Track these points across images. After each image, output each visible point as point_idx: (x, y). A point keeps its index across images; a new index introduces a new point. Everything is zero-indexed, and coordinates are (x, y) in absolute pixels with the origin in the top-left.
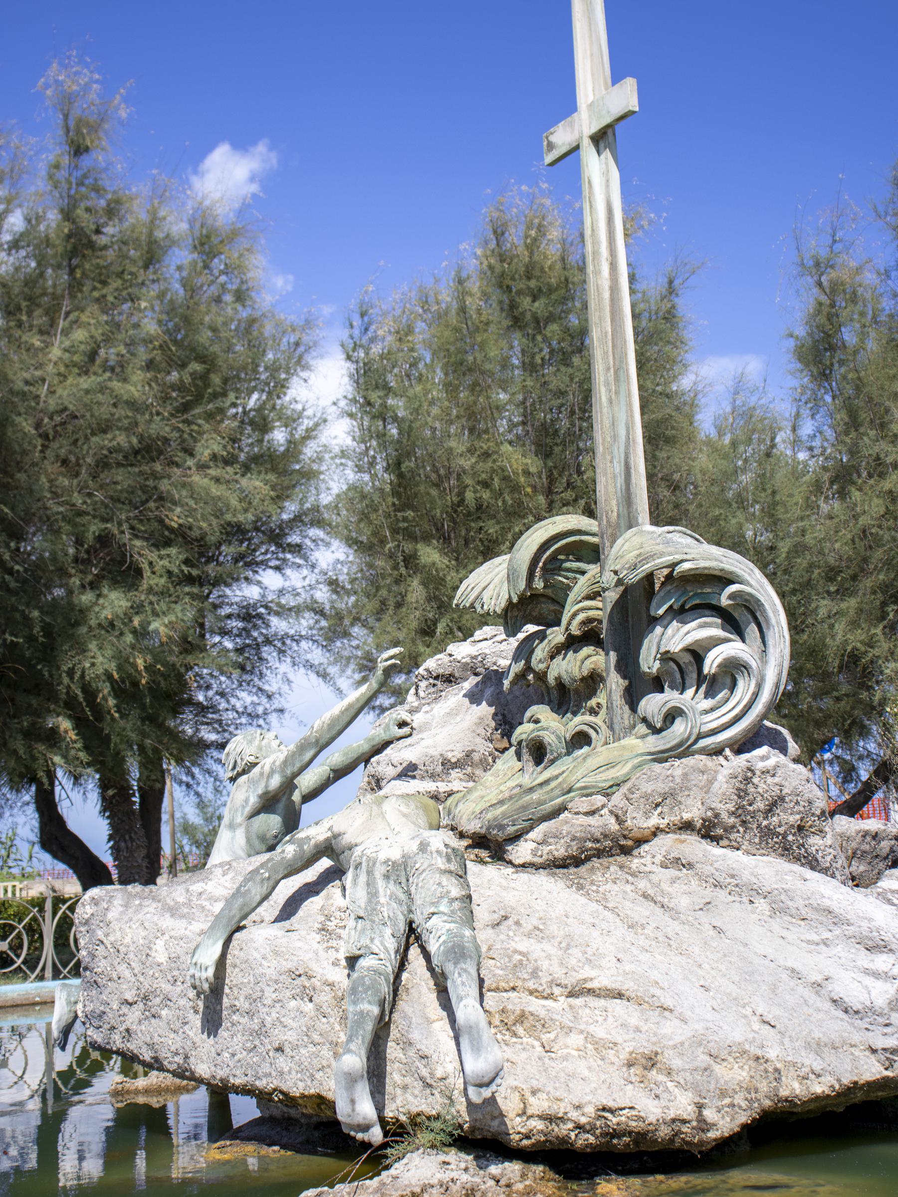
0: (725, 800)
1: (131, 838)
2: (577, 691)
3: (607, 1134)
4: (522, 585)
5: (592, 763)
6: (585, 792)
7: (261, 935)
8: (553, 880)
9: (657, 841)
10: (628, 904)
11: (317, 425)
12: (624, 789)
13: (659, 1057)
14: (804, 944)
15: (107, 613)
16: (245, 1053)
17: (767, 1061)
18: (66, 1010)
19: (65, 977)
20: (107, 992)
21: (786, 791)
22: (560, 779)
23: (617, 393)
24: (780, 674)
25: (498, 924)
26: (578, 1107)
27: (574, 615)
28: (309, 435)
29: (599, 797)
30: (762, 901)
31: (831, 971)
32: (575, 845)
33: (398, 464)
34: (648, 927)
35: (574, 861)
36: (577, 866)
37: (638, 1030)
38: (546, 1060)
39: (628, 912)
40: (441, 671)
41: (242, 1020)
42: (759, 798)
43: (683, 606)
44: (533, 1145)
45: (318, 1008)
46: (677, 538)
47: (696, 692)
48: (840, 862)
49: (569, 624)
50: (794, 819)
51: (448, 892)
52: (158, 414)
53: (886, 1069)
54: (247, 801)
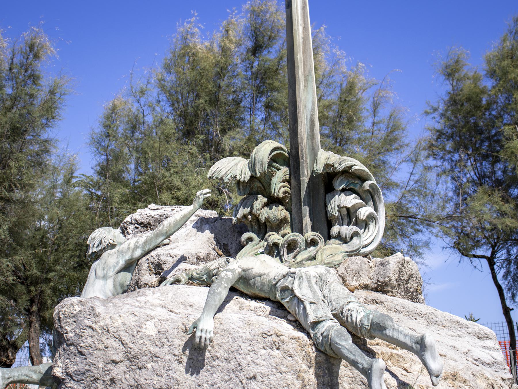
16: (222, 383)
30: (421, 319)
40: (143, 221)
41: (221, 364)
54: (117, 263)
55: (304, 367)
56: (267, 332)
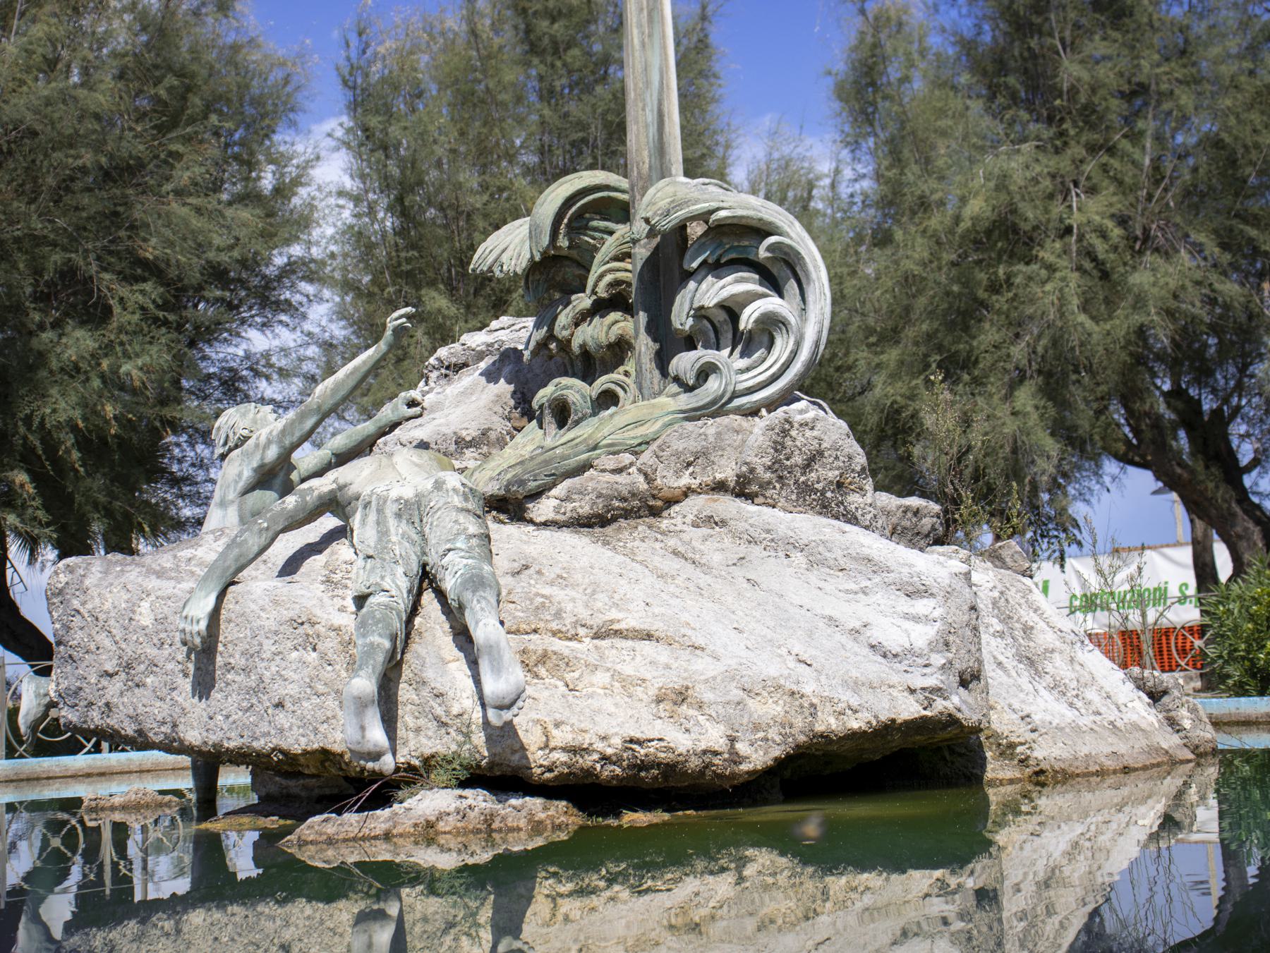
0: (761, 453)
2: (602, 359)
3: (635, 766)
4: (545, 240)
5: (620, 420)
6: (612, 449)
7: (259, 584)
12: (654, 446)
13: (690, 692)
14: (842, 594)
15: (71, 354)
16: (240, 713)
17: (802, 696)
18: (35, 703)
19: (21, 756)
20: (84, 665)
21: (824, 445)
24: (820, 332)
26: (604, 738)
28: (297, 182)
30: (799, 554)
31: (870, 616)
36: (602, 527)
37: (668, 667)
38: (570, 698)
40: (454, 360)
41: (238, 679)
42: (797, 452)
43: (718, 260)
44: (556, 777)
45: (323, 656)
46: (712, 188)
48: (880, 522)
49: (596, 285)
50: (833, 475)
51: (465, 529)
52: (131, 129)
53: (925, 709)
54: (240, 475)
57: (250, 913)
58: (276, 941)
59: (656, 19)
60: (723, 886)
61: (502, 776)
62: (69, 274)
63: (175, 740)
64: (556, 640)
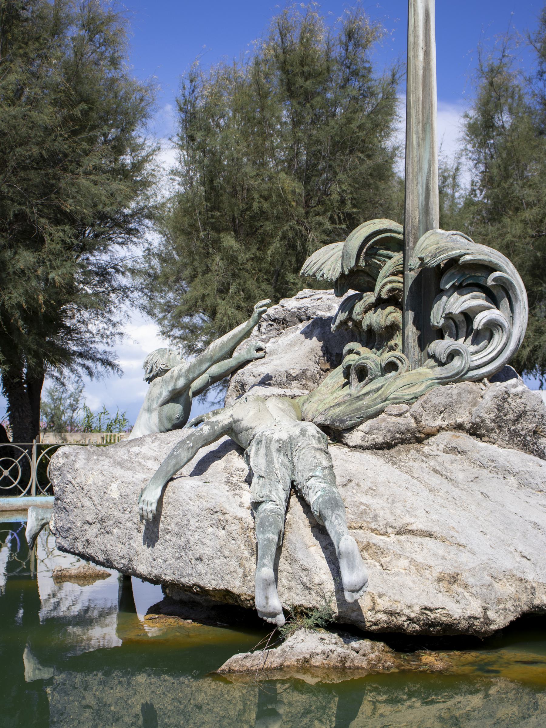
1: (22, 410)
2: (380, 335)
4: (353, 263)
5: (400, 382)
6: (395, 401)
8: (375, 457)
9: (439, 435)
10: (425, 475)
11: (154, 151)
12: (421, 401)
13: (459, 577)
14: (541, 507)
15: (21, 265)
16: (174, 560)
17: (527, 582)
18: (35, 524)
20: (73, 515)
22: (380, 392)
23: (423, 139)
25: (345, 485)
26: (409, 607)
27: (384, 285)
28: (145, 160)
29: (404, 405)
30: (512, 478)
32: (389, 435)
33: (212, 181)
34: (441, 491)
35: (386, 446)
36: (388, 449)
38: (385, 575)
39: (428, 481)
40: (277, 316)
42: (511, 412)
43: (461, 284)
44: (379, 629)
45: (229, 534)
46: (459, 238)
47: (465, 341)
49: (380, 291)
50: (532, 426)
51: (321, 463)
54: (160, 394)
55: (246, 554)
56: (212, 508)
57: (175, 681)
58: (192, 701)
59: (428, 130)
60: (476, 700)
61: (347, 625)
62: (20, 216)
63: (130, 569)
64: (373, 534)
